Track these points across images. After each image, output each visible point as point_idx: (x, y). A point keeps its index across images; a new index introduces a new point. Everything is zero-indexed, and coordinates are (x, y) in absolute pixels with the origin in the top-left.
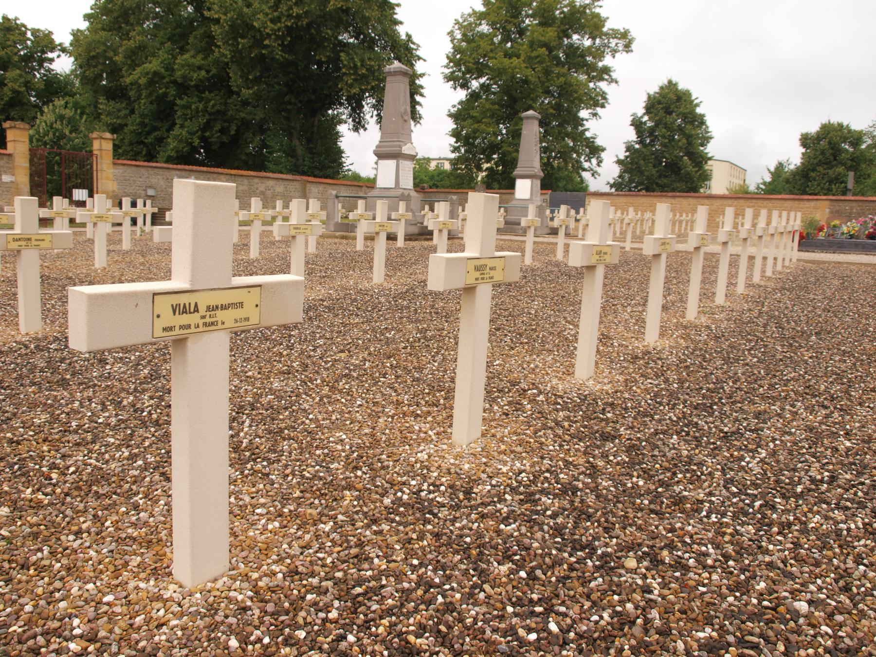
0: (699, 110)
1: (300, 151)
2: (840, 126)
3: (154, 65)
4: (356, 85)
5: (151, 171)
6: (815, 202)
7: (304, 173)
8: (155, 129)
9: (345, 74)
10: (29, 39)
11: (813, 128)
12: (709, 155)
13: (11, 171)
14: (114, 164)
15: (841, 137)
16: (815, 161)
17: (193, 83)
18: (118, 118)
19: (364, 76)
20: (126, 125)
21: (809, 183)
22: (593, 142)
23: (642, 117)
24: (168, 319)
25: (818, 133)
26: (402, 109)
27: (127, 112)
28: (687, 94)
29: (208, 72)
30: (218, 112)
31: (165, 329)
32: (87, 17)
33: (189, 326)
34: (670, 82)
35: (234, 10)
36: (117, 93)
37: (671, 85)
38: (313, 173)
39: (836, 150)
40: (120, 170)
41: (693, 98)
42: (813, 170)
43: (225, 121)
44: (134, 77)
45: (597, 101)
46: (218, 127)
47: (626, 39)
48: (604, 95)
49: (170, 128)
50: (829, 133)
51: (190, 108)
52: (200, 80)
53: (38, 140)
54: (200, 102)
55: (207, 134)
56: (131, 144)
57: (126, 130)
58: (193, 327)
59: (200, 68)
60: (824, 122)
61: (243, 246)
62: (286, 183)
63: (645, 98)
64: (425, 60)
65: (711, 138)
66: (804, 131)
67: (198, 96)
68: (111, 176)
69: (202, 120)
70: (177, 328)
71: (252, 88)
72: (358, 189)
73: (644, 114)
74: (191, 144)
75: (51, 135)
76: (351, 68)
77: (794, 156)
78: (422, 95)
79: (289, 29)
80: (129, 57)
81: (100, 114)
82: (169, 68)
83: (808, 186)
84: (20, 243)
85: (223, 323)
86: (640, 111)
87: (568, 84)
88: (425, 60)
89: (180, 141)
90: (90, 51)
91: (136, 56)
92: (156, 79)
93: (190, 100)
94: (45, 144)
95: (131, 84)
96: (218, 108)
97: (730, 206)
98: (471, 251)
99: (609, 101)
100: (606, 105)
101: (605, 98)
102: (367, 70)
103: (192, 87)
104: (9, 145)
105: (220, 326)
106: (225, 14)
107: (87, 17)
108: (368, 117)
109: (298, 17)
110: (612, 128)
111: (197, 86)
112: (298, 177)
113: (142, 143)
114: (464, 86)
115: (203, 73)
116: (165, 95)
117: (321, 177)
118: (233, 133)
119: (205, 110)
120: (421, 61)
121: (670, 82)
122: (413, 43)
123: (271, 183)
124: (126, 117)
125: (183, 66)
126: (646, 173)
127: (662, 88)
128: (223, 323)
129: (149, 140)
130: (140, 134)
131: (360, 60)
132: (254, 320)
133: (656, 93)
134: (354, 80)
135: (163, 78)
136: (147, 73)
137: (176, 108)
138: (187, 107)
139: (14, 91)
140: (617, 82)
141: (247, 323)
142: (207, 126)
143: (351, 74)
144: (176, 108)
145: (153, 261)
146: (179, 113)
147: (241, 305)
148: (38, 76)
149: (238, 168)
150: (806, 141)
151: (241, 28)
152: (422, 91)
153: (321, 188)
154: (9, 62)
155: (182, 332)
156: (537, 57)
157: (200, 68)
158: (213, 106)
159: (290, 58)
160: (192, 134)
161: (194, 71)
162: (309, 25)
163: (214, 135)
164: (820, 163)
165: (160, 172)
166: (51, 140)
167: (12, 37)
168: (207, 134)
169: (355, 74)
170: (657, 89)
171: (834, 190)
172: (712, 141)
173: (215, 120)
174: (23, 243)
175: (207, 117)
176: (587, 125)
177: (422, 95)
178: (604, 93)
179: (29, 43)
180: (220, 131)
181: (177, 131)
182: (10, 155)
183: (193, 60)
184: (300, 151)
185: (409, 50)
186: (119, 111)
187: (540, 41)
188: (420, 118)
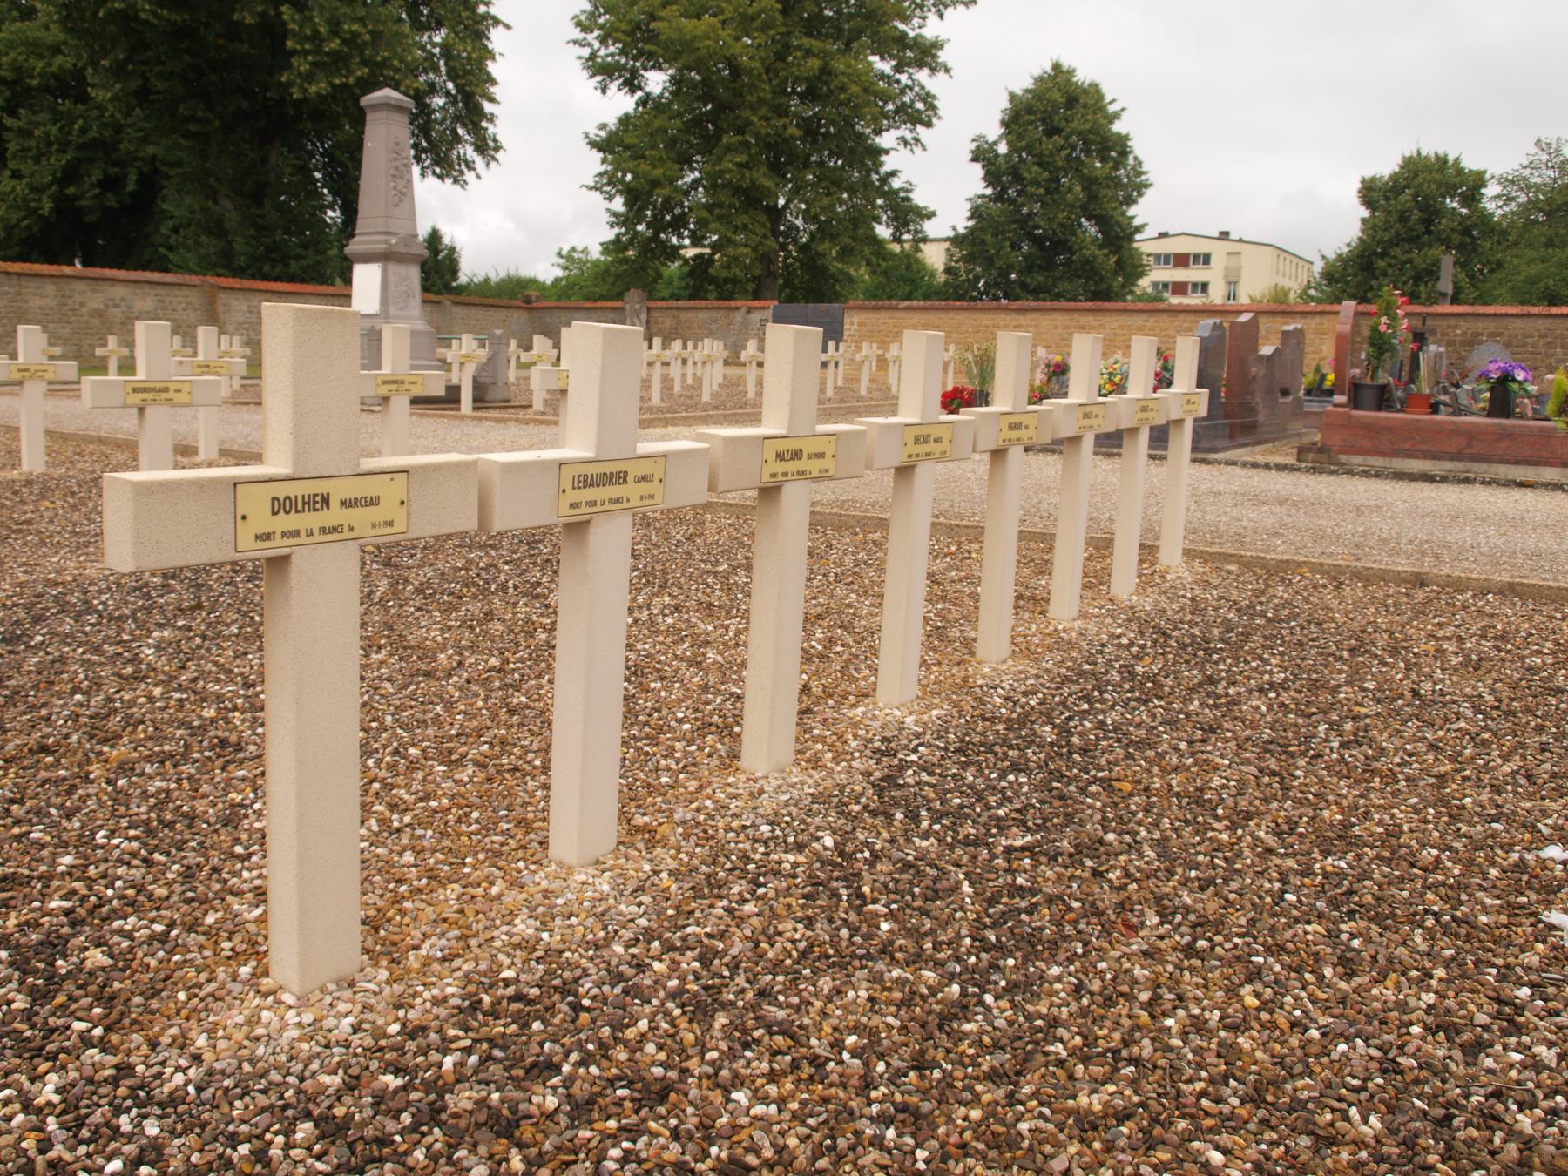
0: (1118, 127)
1: (232, 219)
2: (1442, 161)
4: (321, 76)
6: (1317, 319)
7: (239, 272)
9: (294, 53)
11: (1386, 166)
12: (1136, 222)
15: (1439, 186)
16: (1386, 236)
17: (34, 82)
21: (1374, 283)
22: (908, 199)
23: (995, 143)
24: (262, 519)
25: (1394, 177)
28: (1094, 92)
31: (259, 537)
33: (297, 534)
34: (1057, 67)
37: (1059, 75)
39: (1431, 212)
41: (1108, 98)
42: (1383, 255)
43: (115, 164)
45: (919, 113)
46: (97, 174)
48: (928, 99)
50: (1416, 175)
55: (71, 190)
58: (303, 534)
60: (1407, 154)
61: (823, 391)
62: (160, 291)
64: (508, 27)
65: (1146, 186)
66: (1369, 173)
69: (58, 161)
70: (278, 535)
73: (1001, 137)
74: (35, 210)
76: (307, 38)
77: (1340, 225)
78: (492, 100)
83: (1371, 288)
84: (145, 396)
85: (351, 529)
86: (993, 131)
87: (826, 72)
88: (508, 27)
89: (14, 207)
97: (1141, 331)
99: (940, 112)
100: (934, 120)
101: (932, 107)
102: (344, 42)
103: (37, 90)
105: (347, 534)
110: (940, 176)
111: (45, 89)
112: (194, 279)
114: (632, 85)
117: (278, 279)
118: (131, 187)
120: (501, 27)
121: (1057, 67)
123: (119, 291)
126: (998, 263)
127: (1039, 80)
128: (351, 529)
131: (329, 22)
132: (400, 526)
133: (1027, 91)
134: (315, 64)
137: (6, 135)
138: (26, 133)
140: (947, 70)
141: (389, 530)
142: (71, 174)
143: (307, 52)
144: (7, 135)
145: (738, 405)
147: (374, 502)
149: (144, 267)
150: (1371, 193)
152: (492, 89)
155: (287, 542)
158: (83, 131)
159: (175, 17)
160: (40, 190)
161: (41, 57)
163: (87, 193)
164: (1397, 241)
169: (317, 51)
170: (1028, 83)
171: (1423, 296)
172: (1149, 193)
174: (394, 387)
176: (889, 163)
177: (492, 100)
178: (928, 94)
180: (100, 184)
184: (232, 219)
188: (497, 148)
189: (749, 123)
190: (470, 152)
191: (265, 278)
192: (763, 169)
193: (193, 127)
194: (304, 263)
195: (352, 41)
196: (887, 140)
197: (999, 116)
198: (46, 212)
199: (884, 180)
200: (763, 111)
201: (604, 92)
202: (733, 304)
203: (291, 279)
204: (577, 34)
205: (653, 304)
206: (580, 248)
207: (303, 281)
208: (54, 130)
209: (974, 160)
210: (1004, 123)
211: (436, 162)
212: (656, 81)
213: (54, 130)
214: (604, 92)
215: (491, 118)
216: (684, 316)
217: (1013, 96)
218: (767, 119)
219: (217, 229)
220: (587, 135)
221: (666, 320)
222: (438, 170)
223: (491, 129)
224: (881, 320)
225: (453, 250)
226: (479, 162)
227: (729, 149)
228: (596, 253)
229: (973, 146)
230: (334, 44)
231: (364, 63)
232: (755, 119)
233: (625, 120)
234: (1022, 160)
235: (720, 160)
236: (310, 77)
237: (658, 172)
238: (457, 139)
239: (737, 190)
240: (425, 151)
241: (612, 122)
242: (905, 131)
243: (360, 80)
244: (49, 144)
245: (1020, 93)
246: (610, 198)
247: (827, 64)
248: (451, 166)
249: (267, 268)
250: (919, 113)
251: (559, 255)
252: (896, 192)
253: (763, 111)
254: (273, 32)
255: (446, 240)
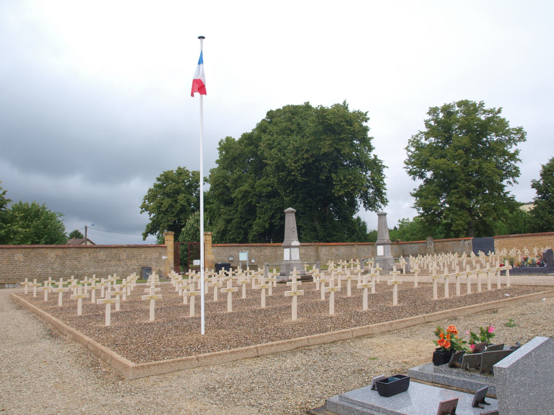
1: (318, 227)
3: (245, 187)
5: (231, 248)
7: (321, 240)
8: (248, 220)
9: (335, 185)
10: (190, 177)
13: (166, 254)
14: (213, 246)
18: (230, 215)
19: (346, 184)
20: (233, 219)
22: (513, 200)
23: (539, 181)
26: (291, 227)
27: (235, 211)
29: (272, 187)
30: (279, 208)
32: (217, 162)
35: (277, 158)
36: (229, 202)
38: (326, 239)
40: (215, 249)
44: (236, 194)
47: (521, 134)
48: (516, 168)
49: (254, 220)
51: (263, 207)
52: (268, 192)
53: (186, 233)
54: (268, 204)
55: (273, 221)
56: (236, 228)
57: (233, 221)
59: (268, 186)
62: (306, 247)
63: (541, 168)
64: (387, 167)
67: (268, 201)
68: (211, 252)
71: (289, 196)
72: (352, 246)
74: (264, 227)
75: (192, 231)
78: (385, 189)
79: (304, 166)
80: (234, 183)
81: (221, 214)
82: (253, 188)
86: (538, 178)
88: (387, 167)
90: (216, 182)
91: (237, 182)
92: (246, 194)
93: (263, 203)
94: (190, 235)
95: (234, 198)
96: (278, 206)
98: (364, 284)
104: (166, 242)
106: (272, 161)
107: (217, 162)
108: (359, 203)
109: (307, 158)
112: (313, 244)
113: (241, 228)
114: (422, 176)
115: (270, 188)
116: (251, 202)
117: (330, 242)
119: (271, 209)
122: (378, 160)
124: (233, 215)
125: (259, 186)
126: (545, 219)
129: (245, 226)
130: (240, 223)
133: (548, 164)
134: (341, 187)
135: (250, 193)
136: (242, 192)
137: (257, 208)
138: (262, 207)
139: (182, 205)
140: (520, 161)
142: (273, 217)
143: (338, 185)
144: (257, 208)
146: (258, 211)
148: (194, 195)
151: (280, 167)
153: (328, 248)
154: (180, 190)
156: (459, 155)
157: (268, 186)
158: (275, 205)
161: (265, 188)
162: (314, 162)
165: (236, 248)
166: (192, 233)
167: (182, 178)
168: (273, 221)
169: (341, 184)
170: (548, 162)
173: (277, 213)
175: (273, 212)
176: (506, 190)
177: (385, 189)
179: (190, 179)
181: (257, 220)
182: (166, 247)
183: (264, 182)
184: (318, 227)
185: (376, 164)
186: (230, 211)
187: (458, 146)
188: (387, 202)
189: (459, 186)
190: (380, 203)
191: (328, 242)
192: (464, 198)
193: (309, 205)
194: (337, 237)
195: (349, 180)
196: (504, 182)
197: (539, 173)
198: (267, 227)
199: (505, 195)
200: (463, 182)
201: (414, 179)
202: (459, 239)
203: (334, 241)
204: (406, 166)
205: (435, 241)
206: (406, 219)
207: (337, 242)
208: (269, 206)
209: (533, 187)
210: (541, 175)
211: (370, 206)
212: (429, 174)
213: (269, 206)
214: (414, 179)
215: (385, 194)
216: (445, 243)
217: (543, 166)
218: (464, 184)
219: (314, 230)
220: (411, 193)
221: (440, 245)
222: (371, 208)
223: (385, 197)
224: (506, 241)
225: (364, 223)
226: (382, 206)
227: (454, 193)
228: (411, 220)
229: (532, 183)
230: (345, 182)
231: (352, 185)
232: (460, 184)
233: (421, 186)
234: (549, 186)
235: (451, 196)
236: (339, 190)
237: (433, 203)
238: (376, 200)
239: (457, 205)
240: (367, 203)
241: (417, 188)
242: (511, 180)
243: (352, 190)
244: (267, 210)
245: (545, 165)
246: (419, 210)
247: (481, 165)
248: (375, 207)
249: (328, 239)
250: (516, 173)
251: (399, 221)
252: (509, 198)
253: (463, 182)
254: (329, 180)
255: (362, 220)
